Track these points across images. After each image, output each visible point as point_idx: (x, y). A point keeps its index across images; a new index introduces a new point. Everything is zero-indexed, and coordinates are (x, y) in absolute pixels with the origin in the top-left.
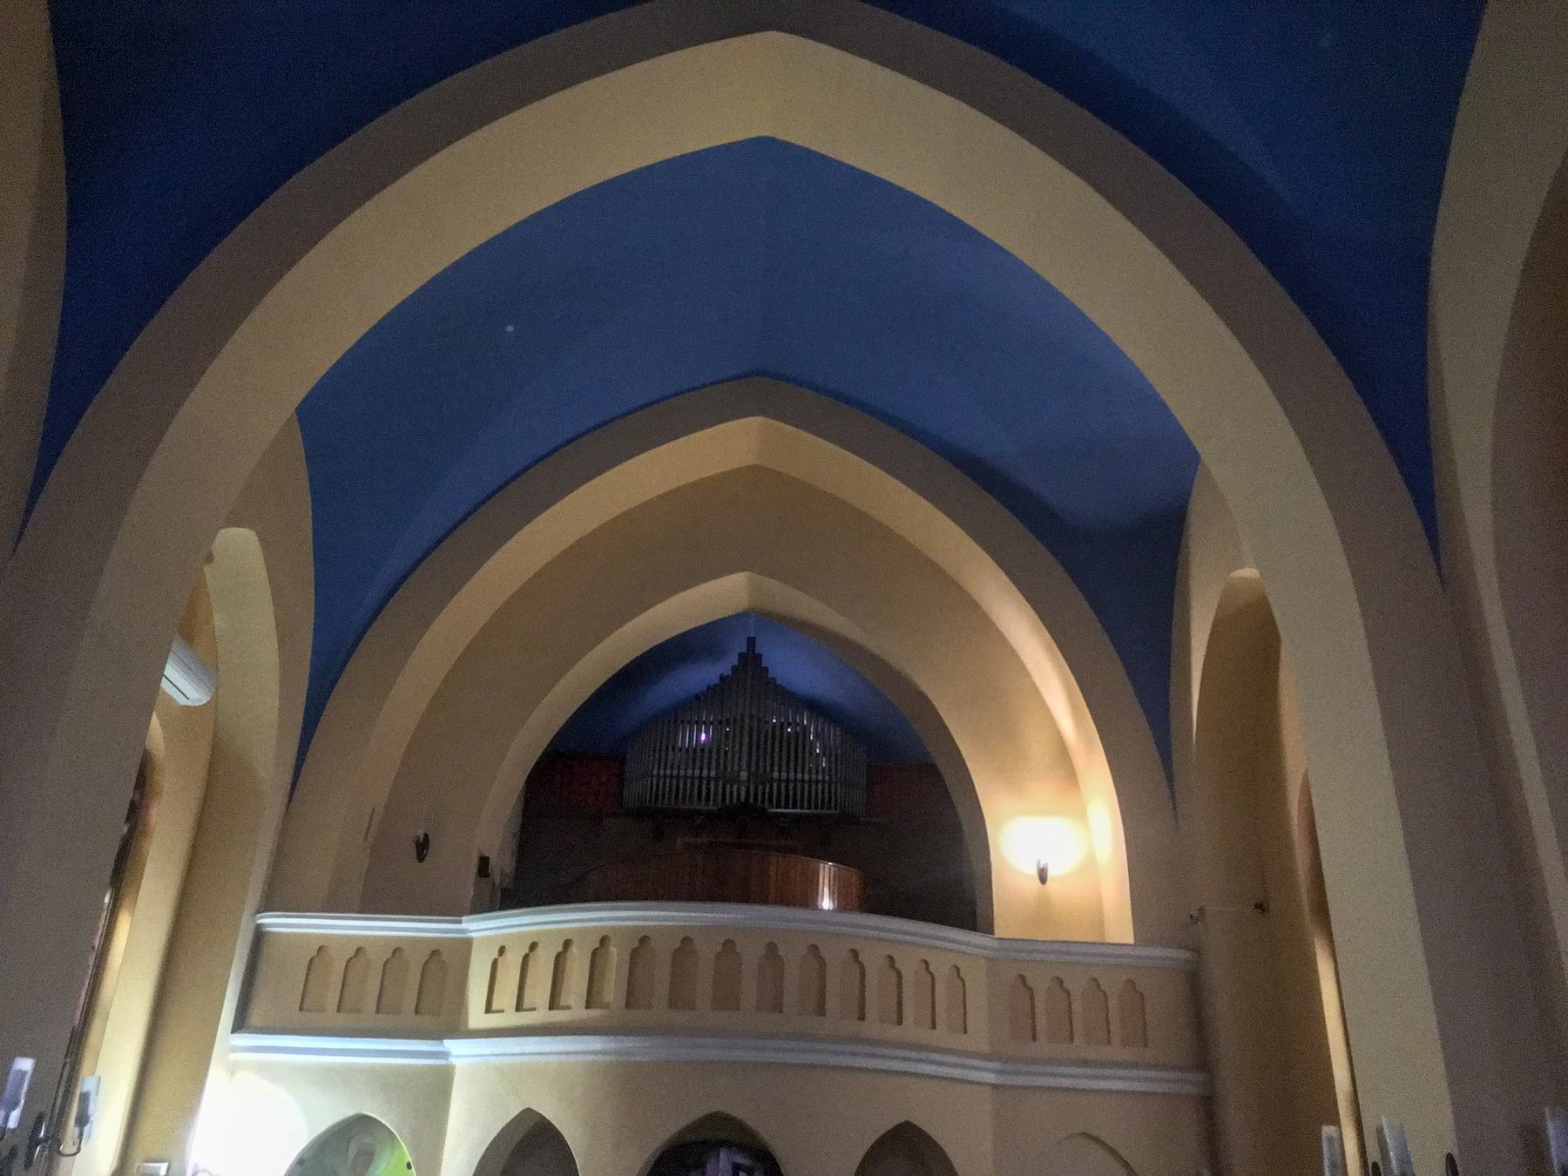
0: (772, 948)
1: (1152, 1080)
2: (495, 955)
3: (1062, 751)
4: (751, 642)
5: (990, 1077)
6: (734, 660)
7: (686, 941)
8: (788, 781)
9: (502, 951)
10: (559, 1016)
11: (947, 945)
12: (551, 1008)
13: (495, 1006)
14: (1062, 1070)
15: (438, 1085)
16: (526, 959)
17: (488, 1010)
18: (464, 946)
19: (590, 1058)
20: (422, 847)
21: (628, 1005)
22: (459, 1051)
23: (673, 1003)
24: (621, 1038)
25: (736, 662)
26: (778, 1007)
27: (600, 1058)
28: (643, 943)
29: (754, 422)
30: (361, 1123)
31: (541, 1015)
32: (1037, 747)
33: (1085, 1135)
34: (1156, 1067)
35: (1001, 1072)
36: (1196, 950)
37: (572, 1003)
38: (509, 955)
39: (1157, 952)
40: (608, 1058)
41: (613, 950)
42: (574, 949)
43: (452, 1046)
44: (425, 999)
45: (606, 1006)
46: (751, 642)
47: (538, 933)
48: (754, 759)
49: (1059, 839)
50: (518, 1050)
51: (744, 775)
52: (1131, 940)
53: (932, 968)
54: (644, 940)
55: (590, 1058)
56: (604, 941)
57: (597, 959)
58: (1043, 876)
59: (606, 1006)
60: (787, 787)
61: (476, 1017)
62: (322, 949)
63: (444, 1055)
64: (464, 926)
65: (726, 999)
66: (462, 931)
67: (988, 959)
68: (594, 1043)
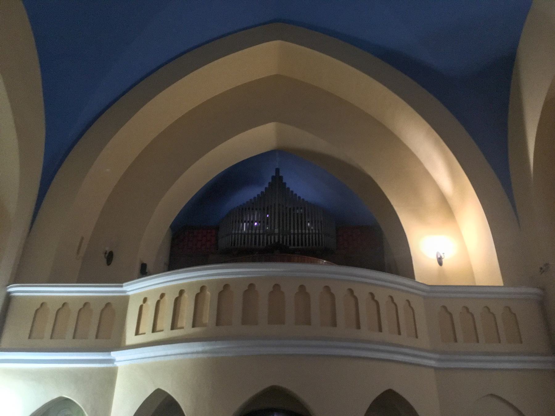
0: (302, 287)
1: (533, 362)
2: (141, 303)
3: (443, 200)
4: (277, 171)
5: (433, 363)
6: (267, 185)
7: (251, 286)
8: (298, 234)
9: (145, 300)
10: (176, 333)
11: (401, 287)
12: (172, 328)
13: (141, 331)
14: (474, 358)
15: (109, 377)
16: (158, 303)
17: (137, 333)
18: (125, 300)
19: (195, 356)
20: (110, 257)
21: (218, 324)
22: (120, 358)
23: (245, 321)
24: (213, 342)
25: (270, 181)
26: (308, 322)
27: (200, 356)
28: (225, 289)
29: (274, 45)
30: (62, 403)
31: (166, 333)
32: (430, 198)
33: (492, 395)
34: (530, 354)
35: (438, 360)
36: (543, 289)
37: (184, 324)
38: (149, 302)
39: (524, 290)
40: (205, 356)
41: (208, 293)
42: (185, 295)
43: (115, 355)
44: (102, 329)
45: (204, 325)
46: (277, 171)
47: (165, 288)
48: (281, 219)
49: (451, 238)
50: (152, 354)
51: (277, 231)
52: (502, 284)
53: (395, 301)
54: (226, 286)
55: (195, 356)
56: (203, 288)
57: (198, 299)
58: (440, 263)
59: (204, 325)
60: (298, 236)
61: (130, 338)
62: (43, 305)
63: (112, 361)
64: (124, 289)
65: (276, 317)
66: (125, 292)
67: (425, 297)
68: (197, 347)
